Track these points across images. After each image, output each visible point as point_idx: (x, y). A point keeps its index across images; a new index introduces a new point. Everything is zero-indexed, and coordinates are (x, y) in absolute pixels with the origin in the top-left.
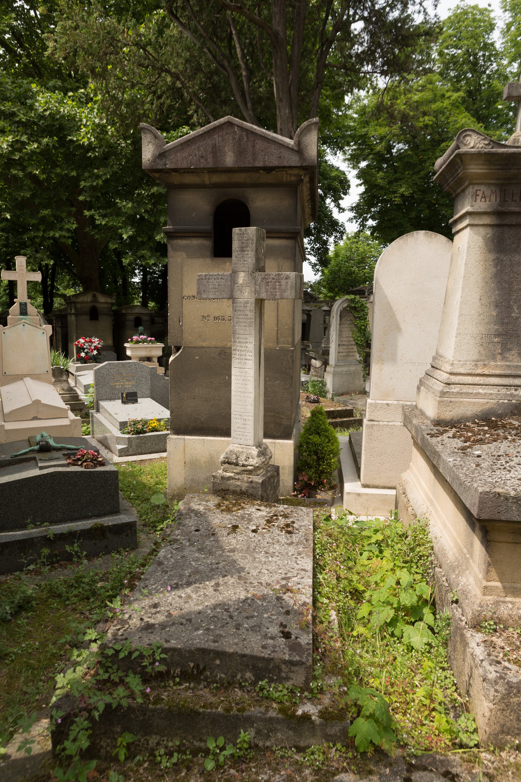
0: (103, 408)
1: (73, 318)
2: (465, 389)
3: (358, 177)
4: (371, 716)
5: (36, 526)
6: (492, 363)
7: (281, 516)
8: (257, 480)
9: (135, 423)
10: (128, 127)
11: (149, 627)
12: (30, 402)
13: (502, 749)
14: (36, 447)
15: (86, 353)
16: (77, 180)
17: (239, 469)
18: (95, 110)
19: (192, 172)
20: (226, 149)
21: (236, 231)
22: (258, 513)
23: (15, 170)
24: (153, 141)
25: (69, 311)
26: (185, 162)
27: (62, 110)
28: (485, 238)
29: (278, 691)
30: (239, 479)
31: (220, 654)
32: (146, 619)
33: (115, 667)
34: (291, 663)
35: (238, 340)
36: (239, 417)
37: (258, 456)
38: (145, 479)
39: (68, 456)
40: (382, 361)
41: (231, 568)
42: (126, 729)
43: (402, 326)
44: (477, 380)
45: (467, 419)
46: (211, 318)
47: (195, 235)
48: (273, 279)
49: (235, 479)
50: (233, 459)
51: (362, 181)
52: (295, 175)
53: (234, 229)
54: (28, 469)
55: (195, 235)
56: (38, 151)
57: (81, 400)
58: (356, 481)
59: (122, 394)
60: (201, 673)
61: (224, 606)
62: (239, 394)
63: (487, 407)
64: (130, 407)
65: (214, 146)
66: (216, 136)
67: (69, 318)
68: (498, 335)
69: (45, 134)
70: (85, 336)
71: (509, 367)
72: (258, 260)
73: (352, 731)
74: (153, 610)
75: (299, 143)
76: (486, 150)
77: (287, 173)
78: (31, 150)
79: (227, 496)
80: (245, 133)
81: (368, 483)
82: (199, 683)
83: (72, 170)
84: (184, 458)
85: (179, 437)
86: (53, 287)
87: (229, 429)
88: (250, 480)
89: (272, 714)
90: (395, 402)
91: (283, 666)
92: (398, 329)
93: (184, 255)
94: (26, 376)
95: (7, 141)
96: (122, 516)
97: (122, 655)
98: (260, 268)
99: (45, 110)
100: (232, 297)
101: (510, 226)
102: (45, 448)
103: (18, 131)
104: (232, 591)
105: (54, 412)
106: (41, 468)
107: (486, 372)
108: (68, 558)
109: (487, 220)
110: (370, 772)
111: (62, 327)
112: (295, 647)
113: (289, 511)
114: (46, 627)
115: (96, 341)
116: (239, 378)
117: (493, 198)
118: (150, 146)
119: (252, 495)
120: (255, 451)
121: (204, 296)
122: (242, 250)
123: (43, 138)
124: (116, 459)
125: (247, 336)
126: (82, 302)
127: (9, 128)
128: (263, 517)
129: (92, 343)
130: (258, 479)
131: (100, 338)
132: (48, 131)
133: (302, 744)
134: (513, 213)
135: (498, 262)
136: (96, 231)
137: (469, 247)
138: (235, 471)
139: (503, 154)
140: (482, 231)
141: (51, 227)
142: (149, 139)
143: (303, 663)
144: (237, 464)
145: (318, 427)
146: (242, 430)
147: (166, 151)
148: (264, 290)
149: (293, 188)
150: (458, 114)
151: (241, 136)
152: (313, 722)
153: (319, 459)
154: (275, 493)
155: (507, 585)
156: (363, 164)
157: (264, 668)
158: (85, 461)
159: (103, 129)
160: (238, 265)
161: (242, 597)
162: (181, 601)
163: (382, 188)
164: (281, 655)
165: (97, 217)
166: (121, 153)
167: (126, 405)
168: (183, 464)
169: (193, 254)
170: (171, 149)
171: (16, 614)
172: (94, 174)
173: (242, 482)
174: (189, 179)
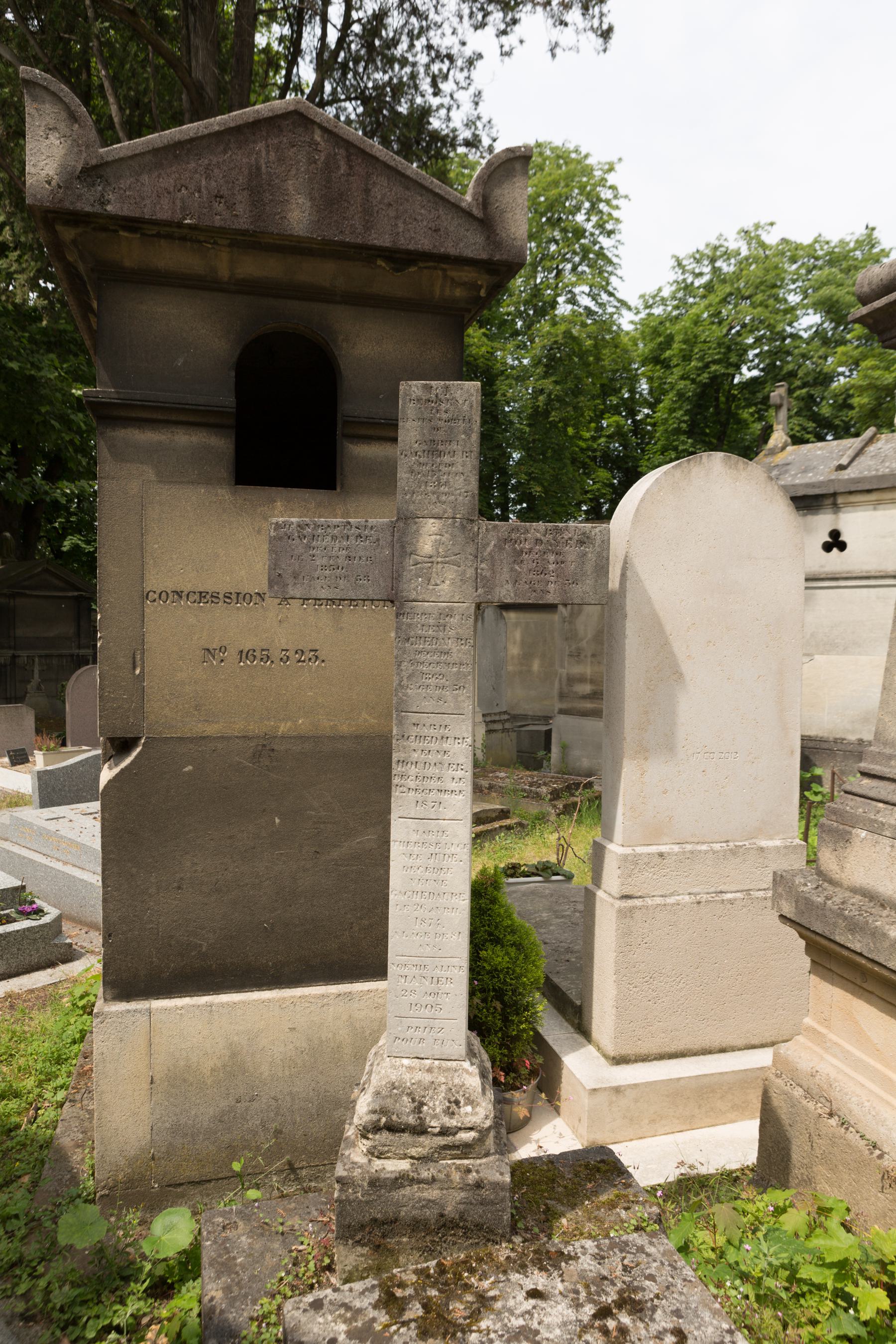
8: (497, 1177)
19: (183, 239)
24: (62, 126)
26: (165, 202)
35: (414, 731)
36: (415, 971)
40: (644, 752)
43: (686, 668)
46: (231, 654)
47: (182, 418)
48: (538, 541)
49: (420, 1181)
50: (405, 1114)
52: (464, 284)
53: (403, 386)
55: (182, 418)
58: (582, 1046)
62: (417, 899)
65: (255, 172)
66: (260, 146)
77: (445, 277)
79: (391, 1242)
80: (342, 152)
81: (627, 1050)
84: (150, 1066)
85: (133, 1005)
88: (472, 1177)
90: (676, 848)
92: (678, 675)
93: (150, 473)
100: (394, 599)
116: (416, 850)
118: (54, 139)
119: (479, 1227)
121: (296, 592)
122: (433, 449)
125: (447, 719)
138: (413, 1152)
142: (50, 120)
144: (420, 1130)
146: (427, 1013)
147: (107, 164)
148: (506, 575)
160: (418, 498)
168: (146, 1086)
170: (121, 160)
174: (171, 258)
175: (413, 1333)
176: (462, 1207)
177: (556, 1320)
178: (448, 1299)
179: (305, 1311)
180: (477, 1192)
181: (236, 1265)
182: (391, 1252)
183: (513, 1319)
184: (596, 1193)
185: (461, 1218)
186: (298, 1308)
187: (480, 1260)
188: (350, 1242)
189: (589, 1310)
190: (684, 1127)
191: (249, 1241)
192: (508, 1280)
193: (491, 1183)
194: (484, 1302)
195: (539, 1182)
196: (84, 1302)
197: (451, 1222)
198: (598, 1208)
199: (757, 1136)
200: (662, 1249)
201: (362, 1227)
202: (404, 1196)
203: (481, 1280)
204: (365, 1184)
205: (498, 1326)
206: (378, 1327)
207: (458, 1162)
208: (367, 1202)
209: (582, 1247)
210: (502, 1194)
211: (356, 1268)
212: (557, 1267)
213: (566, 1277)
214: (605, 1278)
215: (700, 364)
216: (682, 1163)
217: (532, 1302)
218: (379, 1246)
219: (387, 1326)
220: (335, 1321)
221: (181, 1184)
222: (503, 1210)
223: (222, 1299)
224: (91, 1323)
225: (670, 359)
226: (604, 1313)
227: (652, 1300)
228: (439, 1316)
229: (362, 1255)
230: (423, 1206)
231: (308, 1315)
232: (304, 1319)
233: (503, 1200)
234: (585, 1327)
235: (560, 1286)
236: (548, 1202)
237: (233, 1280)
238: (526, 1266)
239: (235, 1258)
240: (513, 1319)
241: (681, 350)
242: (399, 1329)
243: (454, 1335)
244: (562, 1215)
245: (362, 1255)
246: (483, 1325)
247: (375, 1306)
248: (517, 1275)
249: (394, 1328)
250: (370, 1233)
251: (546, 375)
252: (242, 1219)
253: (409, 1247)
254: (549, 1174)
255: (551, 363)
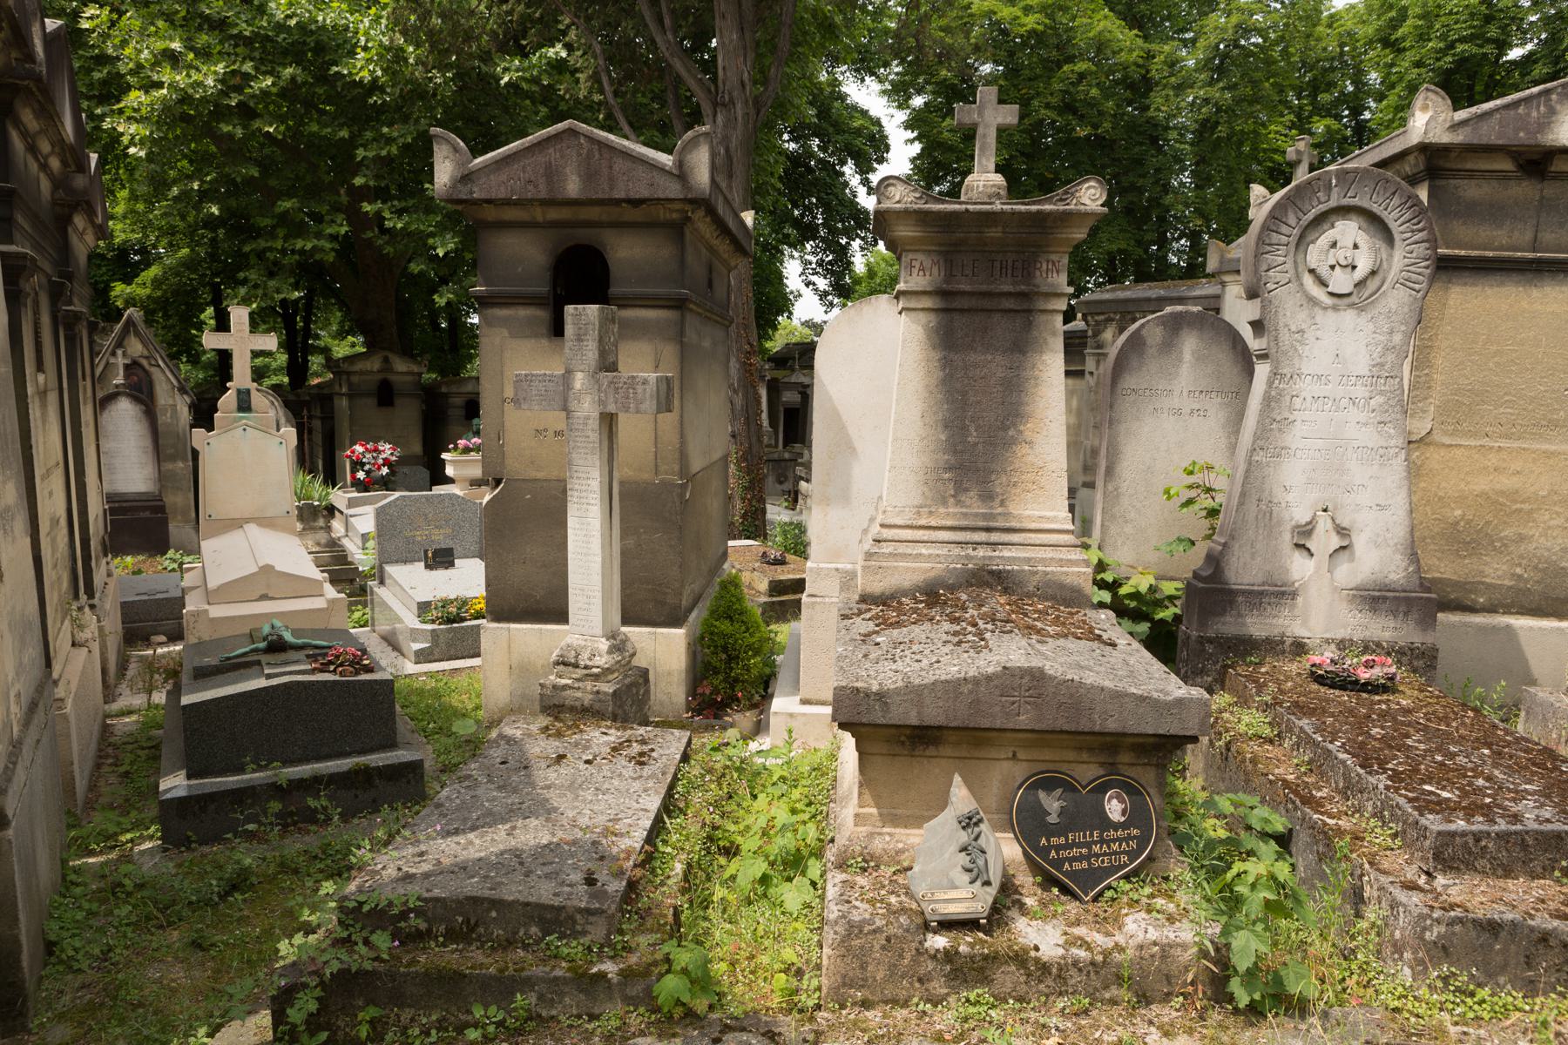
0: (391, 577)
1: (344, 402)
2: (902, 549)
3: (908, 125)
4: (685, 971)
5: (261, 768)
6: (942, 510)
9: (446, 603)
10: (447, 52)
11: (408, 878)
12: (254, 569)
13: (842, 1007)
14: (262, 645)
15: (368, 473)
16: (352, 143)
17: (580, 673)
18: (384, 21)
20: (568, 170)
21: (569, 309)
22: (600, 737)
23: (228, 123)
25: (337, 388)
27: (320, 18)
28: (926, 327)
29: (572, 949)
31: (496, 903)
32: (405, 869)
33: (358, 926)
34: (588, 912)
37: (610, 652)
38: (455, 701)
39: (313, 658)
40: (826, 501)
41: (546, 811)
42: (371, 1001)
43: (858, 444)
44: (919, 534)
45: (905, 593)
46: (550, 433)
51: (916, 134)
54: (248, 679)
56: (274, 90)
57: (351, 563)
59: (426, 552)
60: (472, 930)
61: (517, 854)
63: (932, 574)
64: (440, 574)
65: (549, 166)
66: (551, 150)
67: (336, 401)
68: (949, 469)
69: (289, 59)
70: (365, 440)
71: (965, 515)
72: (603, 353)
73: (656, 989)
74: (417, 859)
75: (680, 164)
76: (916, 207)
78: (261, 89)
82: (470, 944)
83: (341, 126)
86: (307, 333)
87: (567, 613)
89: (558, 973)
91: (578, 917)
92: (852, 450)
93: (505, 333)
94: (248, 521)
95: (215, 73)
96: (400, 753)
97: (366, 908)
98: (608, 365)
99: (289, 17)
100: (565, 408)
101: (962, 311)
102: (277, 647)
103: (237, 55)
104: (532, 834)
105: (300, 586)
106: (269, 677)
107: (933, 523)
108: (311, 817)
109: (927, 303)
110: (674, 1035)
111: (322, 419)
112: (601, 895)
113: (651, 735)
114: (272, 911)
115: (387, 449)
117: (935, 271)
120: (604, 645)
123: (285, 66)
124: (410, 667)
126: (362, 373)
127: (218, 48)
128: (607, 743)
129: (380, 452)
130: (608, 688)
131: (395, 444)
132: (294, 53)
133: (596, 1011)
134: (963, 293)
135: (946, 363)
136: (386, 237)
137: (904, 341)
139: (939, 213)
140: (923, 317)
141: (299, 230)
143: (603, 912)
144: (576, 666)
145: (729, 608)
149: (676, 230)
150: (1093, 11)
151: (590, 151)
152: (609, 981)
153: (730, 659)
154: (641, 710)
155: (885, 811)
156: (918, 101)
157: (555, 920)
158: (341, 665)
159: (399, 55)
161: (545, 842)
162: (459, 848)
163: (951, 149)
164: (576, 903)
165: (387, 215)
166: (435, 95)
167: (434, 572)
169: (520, 331)
171: (223, 896)
172: (383, 135)
173: (584, 694)
215: (1441, 45)
225: (1404, 39)
241: (1416, 27)
251: (1211, 83)
255: (1220, 65)
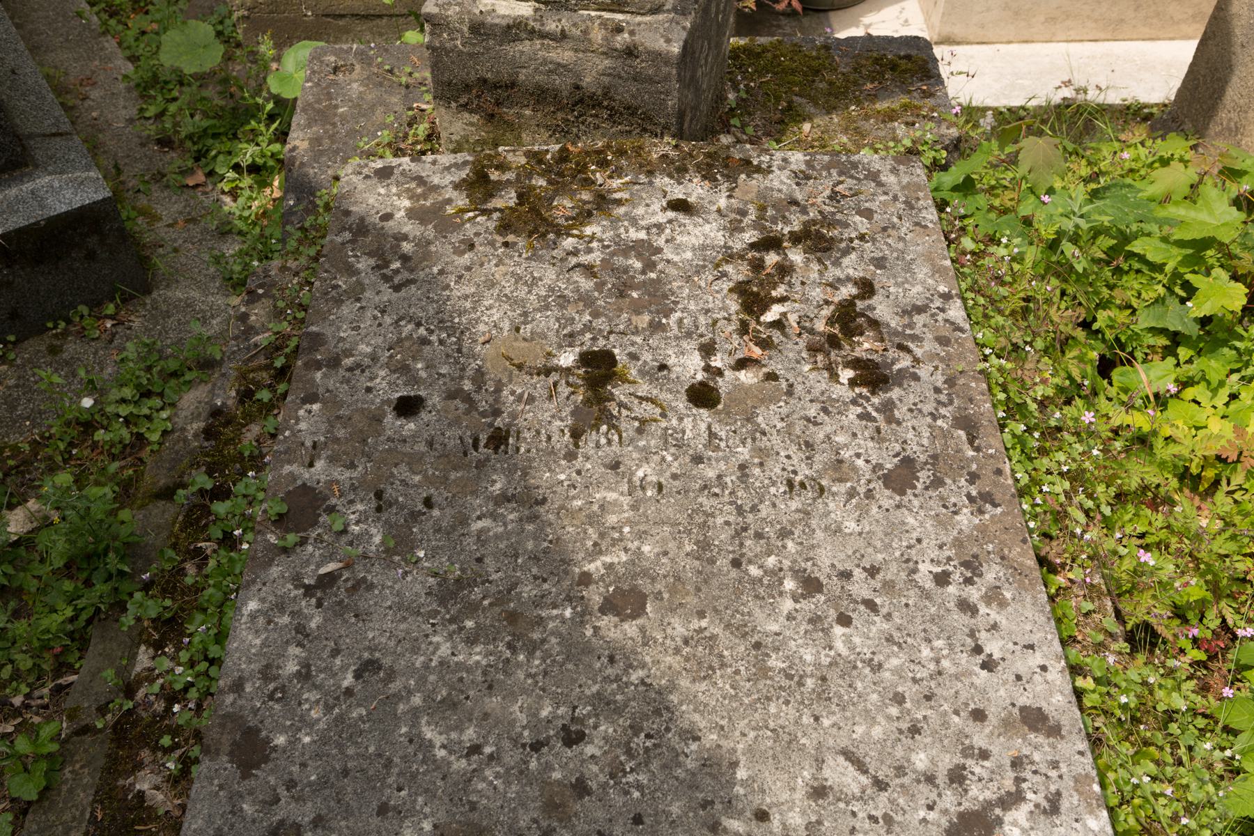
7: (796, 239)
8: (661, 45)
30: (563, 36)
49: (544, 36)
79: (510, 113)
88: (622, 39)
96: (43, 181)
119: (631, 110)
175: (491, 225)
176: (606, 80)
177: (694, 240)
178: (556, 193)
179: (367, 177)
180: (629, 62)
181: (335, 115)
182: (510, 126)
183: (632, 230)
184: (873, 97)
185: (605, 94)
186: (360, 173)
187: (621, 153)
188: (453, 105)
189: (750, 236)
190: (1102, 36)
191: (361, 89)
192: (651, 183)
193: (649, 52)
194: (603, 202)
195: (793, 72)
196: (215, 136)
197: (591, 98)
198: (867, 117)
199: (1190, 60)
200: (905, 180)
201: (467, 88)
202: (522, 52)
203: (610, 177)
204: (466, 29)
205: (609, 234)
206: (450, 210)
207: (606, 15)
208: (471, 55)
209: (785, 160)
210: (665, 70)
211: (466, 139)
212: (731, 178)
213: (737, 193)
214: (794, 202)
216: (1068, 83)
217: (671, 214)
218: (492, 116)
219: (462, 211)
220: (399, 196)
221: (342, 16)
222: (667, 93)
223: (305, 150)
224: (221, 158)
226: (770, 243)
227: (851, 240)
228: (534, 210)
229: (472, 124)
230: (550, 71)
231: (369, 182)
232: (361, 186)
233: (667, 78)
234: (731, 256)
235: (723, 202)
236: (795, 98)
237: (326, 132)
238: (686, 170)
239: (336, 107)
240: (632, 230)
242: (475, 217)
243: (544, 235)
244: (809, 118)
245: (472, 124)
246: (588, 230)
247: (456, 186)
248: (666, 179)
249: (471, 214)
250: (478, 97)
252: (362, 61)
253: (533, 122)
254: (815, 63)
